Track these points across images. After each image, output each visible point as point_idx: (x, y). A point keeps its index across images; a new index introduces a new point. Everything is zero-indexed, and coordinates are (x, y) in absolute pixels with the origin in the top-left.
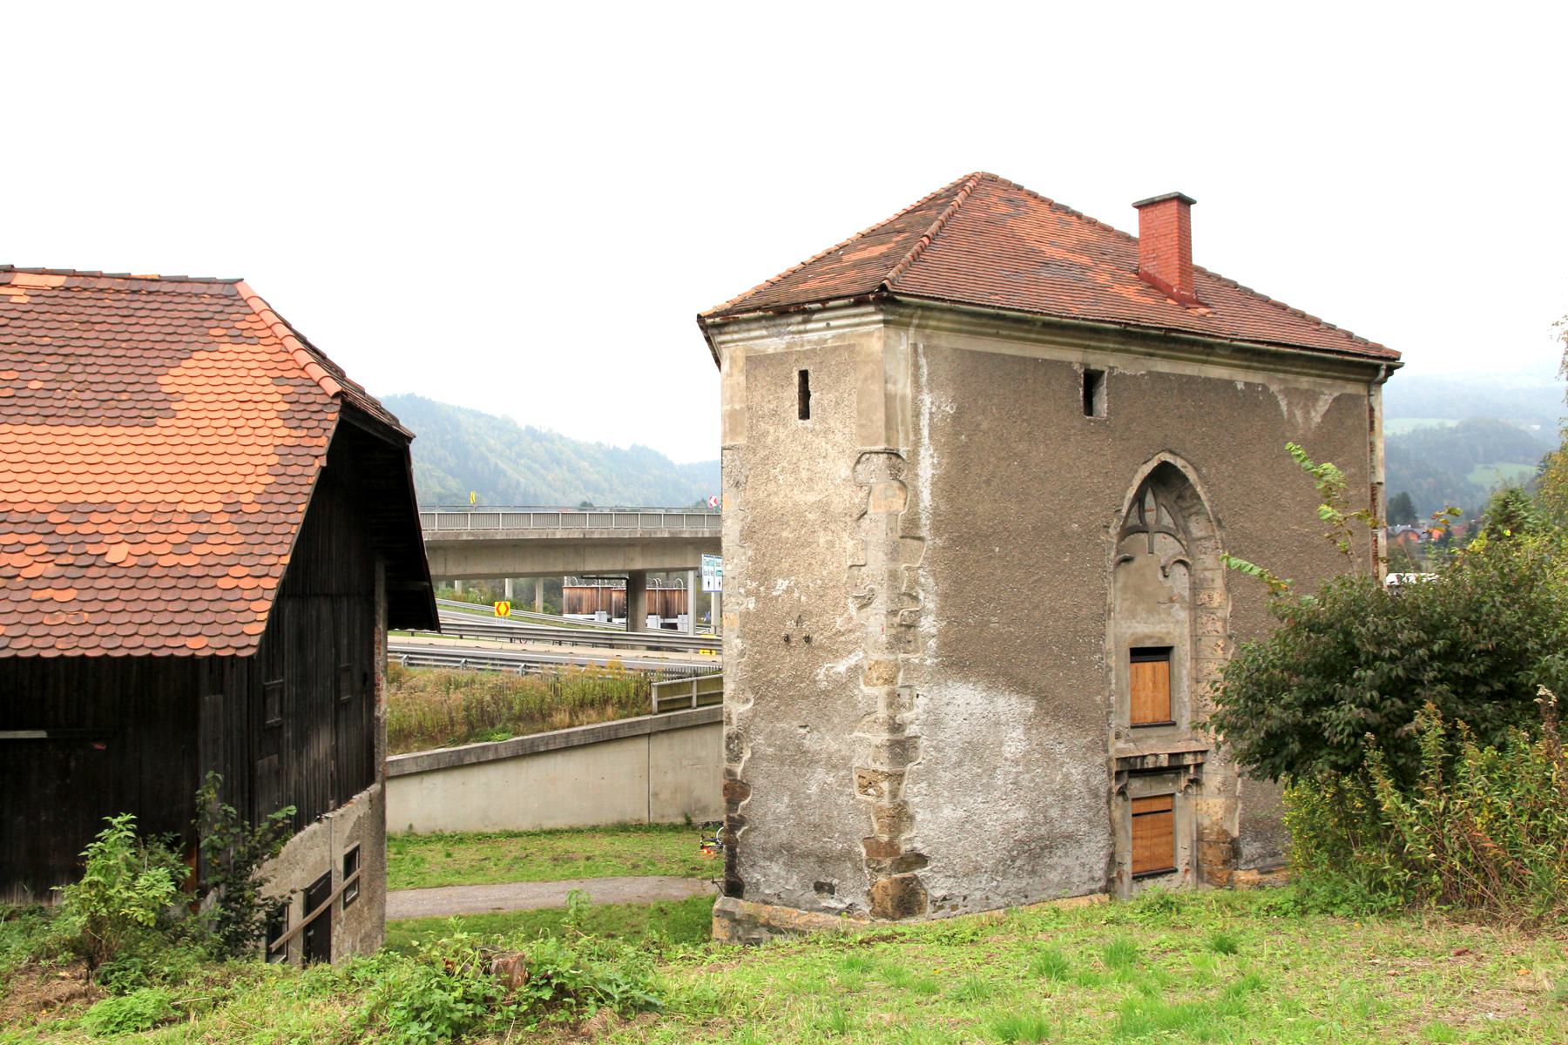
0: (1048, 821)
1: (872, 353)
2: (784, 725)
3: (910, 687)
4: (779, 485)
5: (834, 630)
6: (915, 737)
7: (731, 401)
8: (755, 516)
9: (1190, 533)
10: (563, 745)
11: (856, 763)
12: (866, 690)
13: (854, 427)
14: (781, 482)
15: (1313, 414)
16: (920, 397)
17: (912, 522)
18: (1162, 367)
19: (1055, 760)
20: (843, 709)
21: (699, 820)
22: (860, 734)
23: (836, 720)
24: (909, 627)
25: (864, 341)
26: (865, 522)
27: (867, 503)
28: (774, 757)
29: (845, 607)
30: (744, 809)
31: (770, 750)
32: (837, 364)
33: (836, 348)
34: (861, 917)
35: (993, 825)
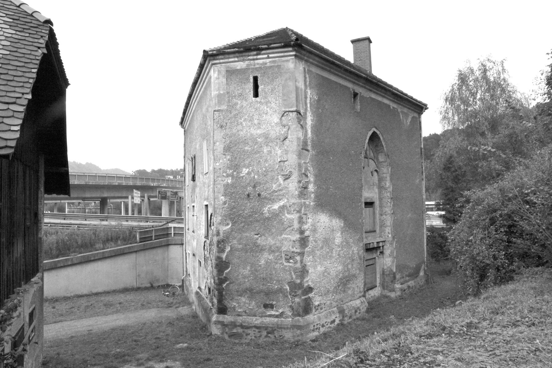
0: (348, 270)
1: (289, 69)
2: (248, 234)
3: (306, 214)
4: (243, 127)
8: (231, 141)
9: (379, 160)
10: (101, 257)
11: (284, 249)
12: (289, 216)
13: (281, 100)
14: (244, 125)
17: (305, 143)
18: (373, 96)
19: (350, 245)
21: (156, 285)
22: (286, 236)
23: (274, 230)
25: (285, 64)
26: (287, 142)
27: (287, 134)
28: (242, 249)
29: (278, 179)
30: (226, 274)
31: (240, 246)
32: (272, 74)
33: (271, 66)
34: (287, 317)
35: (333, 273)
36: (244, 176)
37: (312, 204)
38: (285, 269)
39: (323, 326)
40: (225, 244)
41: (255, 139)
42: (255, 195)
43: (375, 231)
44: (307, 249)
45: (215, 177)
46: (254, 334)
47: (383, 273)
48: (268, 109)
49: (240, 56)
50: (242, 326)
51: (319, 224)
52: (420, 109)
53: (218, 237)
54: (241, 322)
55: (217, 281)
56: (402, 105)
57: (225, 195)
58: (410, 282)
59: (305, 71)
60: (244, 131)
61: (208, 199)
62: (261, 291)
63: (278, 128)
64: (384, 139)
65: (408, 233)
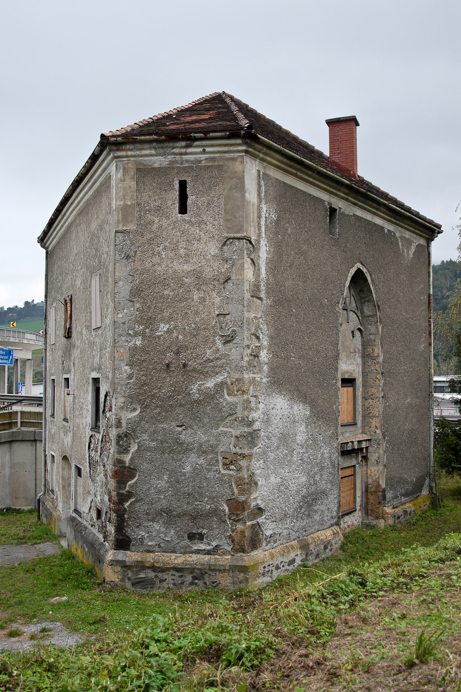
0: (315, 483)
1: (236, 172)
2: (165, 426)
3: (256, 396)
4: (162, 259)
8: (142, 280)
13: (221, 220)
14: (164, 256)
15: (410, 253)
16: (261, 205)
18: (359, 213)
19: (318, 445)
22: (225, 429)
23: (206, 420)
25: (230, 163)
26: (230, 285)
29: (214, 342)
30: (131, 486)
31: (153, 444)
32: (209, 178)
33: (208, 167)
34: (224, 554)
35: (293, 488)
36: (162, 335)
37: (264, 380)
39: (277, 568)
40: (130, 440)
41: (180, 279)
42: (178, 366)
43: (355, 424)
44: (256, 450)
45: (116, 335)
46: (173, 579)
47: (366, 490)
48: (201, 233)
49: (159, 148)
50: (153, 568)
51: (273, 412)
52: (430, 233)
53: (119, 429)
54: (152, 561)
55: (115, 499)
56: (402, 227)
58: (408, 505)
59: (259, 175)
61: (100, 369)
62: (185, 514)
64: (372, 280)
65: (406, 427)
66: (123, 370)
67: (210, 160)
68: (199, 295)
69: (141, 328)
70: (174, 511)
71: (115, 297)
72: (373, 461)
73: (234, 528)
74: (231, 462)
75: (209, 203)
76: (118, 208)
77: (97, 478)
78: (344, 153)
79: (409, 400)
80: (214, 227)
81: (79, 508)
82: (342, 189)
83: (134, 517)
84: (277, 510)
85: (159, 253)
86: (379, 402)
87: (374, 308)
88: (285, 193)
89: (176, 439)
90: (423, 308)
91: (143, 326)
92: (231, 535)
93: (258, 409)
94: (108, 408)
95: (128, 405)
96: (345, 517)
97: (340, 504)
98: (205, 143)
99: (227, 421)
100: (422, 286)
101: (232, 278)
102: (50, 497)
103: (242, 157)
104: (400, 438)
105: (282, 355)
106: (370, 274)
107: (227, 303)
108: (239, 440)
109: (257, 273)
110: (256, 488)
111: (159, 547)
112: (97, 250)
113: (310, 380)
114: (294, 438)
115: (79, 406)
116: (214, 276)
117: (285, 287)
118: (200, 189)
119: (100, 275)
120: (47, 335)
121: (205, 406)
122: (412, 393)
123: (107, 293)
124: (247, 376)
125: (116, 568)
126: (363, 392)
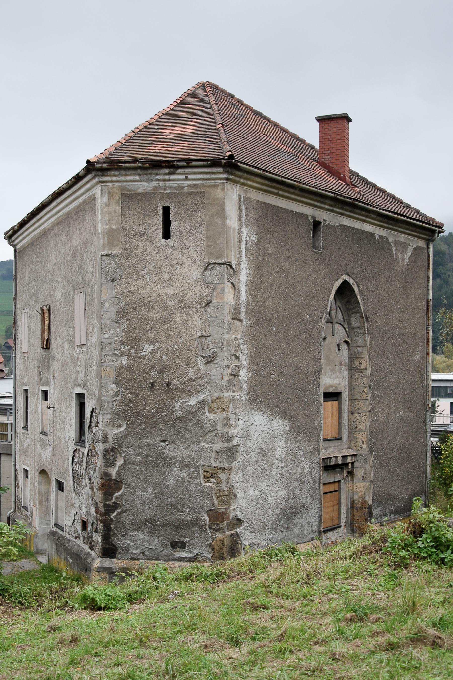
0: (295, 496)
1: (217, 199)
2: (150, 441)
3: (235, 414)
5: (187, 378)
6: (237, 445)
7: (109, 222)
11: (202, 463)
14: (148, 280)
15: (405, 257)
16: (242, 230)
18: (346, 222)
20: (193, 429)
22: (206, 444)
23: (188, 436)
24: (234, 376)
25: (211, 190)
26: (211, 309)
29: (196, 363)
30: (117, 498)
31: (139, 458)
32: (192, 204)
33: (191, 193)
34: (204, 561)
35: (272, 501)
36: (146, 355)
37: (243, 398)
38: (203, 492)
40: (116, 454)
41: (164, 302)
42: (162, 385)
43: (340, 439)
44: (235, 464)
45: (103, 355)
47: (352, 506)
48: (184, 258)
49: (143, 174)
51: (253, 428)
52: (430, 234)
53: (106, 444)
55: (102, 509)
57: (116, 383)
59: (240, 200)
60: (148, 289)
63: (198, 288)
64: (359, 291)
65: (397, 442)
66: (110, 388)
67: (193, 187)
68: (182, 318)
69: (127, 348)
70: (158, 521)
71: (101, 319)
72: (359, 476)
73: (214, 537)
74: (212, 475)
75: (191, 229)
76: (104, 232)
77: (82, 491)
78: (334, 154)
79: (401, 414)
80: (196, 252)
81: (60, 523)
82: (327, 201)
83: (120, 527)
84: (256, 522)
85: (143, 277)
86: (365, 417)
87: (362, 319)
88: (266, 214)
89: (160, 453)
90: (420, 315)
91: (129, 347)
92: (211, 543)
93: (237, 425)
94: (94, 423)
95: (114, 421)
96: (329, 533)
97: (321, 518)
98: (187, 170)
99: (208, 437)
100: (420, 292)
101: (213, 302)
102: (21, 514)
103: (223, 184)
104: (390, 454)
105: (262, 373)
106: (358, 285)
107: (208, 326)
108: (219, 455)
109: (237, 297)
110: (235, 500)
111: (144, 555)
112: (80, 267)
113: (290, 396)
114: (273, 453)
115: (60, 419)
116: (196, 299)
117: (265, 307)
118: (183, 215)
119: (85, 293)
120: (17, 341)
121: (187, 422)
122: (405, 406)
123: (93, 313)
124: (227, 395)
125: (103, 574)
126: (350, 405)
